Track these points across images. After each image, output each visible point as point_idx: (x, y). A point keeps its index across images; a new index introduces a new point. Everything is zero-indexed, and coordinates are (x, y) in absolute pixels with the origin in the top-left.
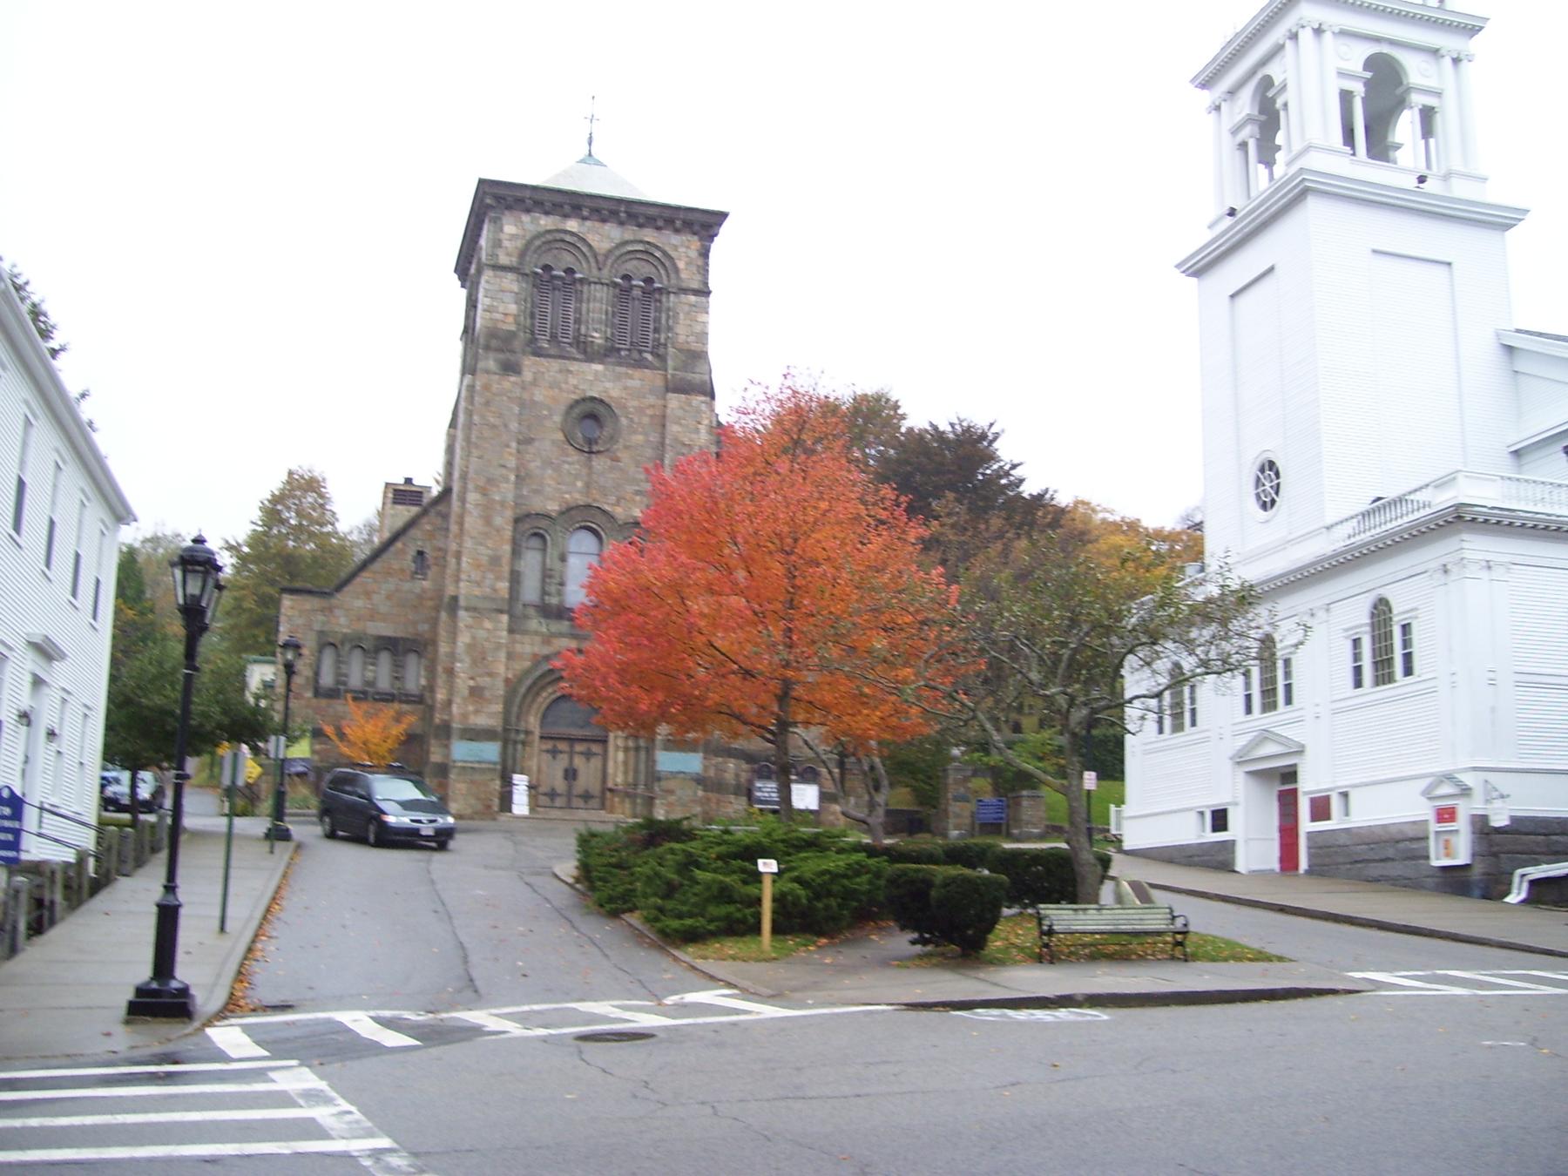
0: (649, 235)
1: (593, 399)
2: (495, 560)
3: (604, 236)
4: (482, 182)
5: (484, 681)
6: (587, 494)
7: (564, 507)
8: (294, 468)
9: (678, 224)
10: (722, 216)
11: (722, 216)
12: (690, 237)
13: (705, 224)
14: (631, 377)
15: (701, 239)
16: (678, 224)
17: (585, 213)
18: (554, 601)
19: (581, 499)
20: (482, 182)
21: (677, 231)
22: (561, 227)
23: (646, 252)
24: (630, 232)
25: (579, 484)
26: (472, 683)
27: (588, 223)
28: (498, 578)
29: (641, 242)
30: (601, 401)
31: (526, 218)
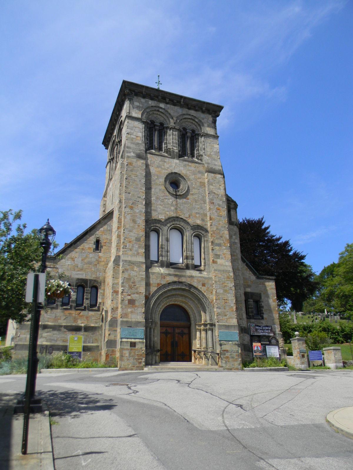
0: (192, 112)
1: (176, 173)
2: (138, 240)
3: (175, 111)
4: (124, 82)
5: (135, 296)
6: (176, 212)
7: (167, 217)
8: (291, 242)
9: (160, 97)
10: (221, 108)
11: (221, 108)
12: (208, 115)
13: (214, 110)
14: (190, 166)
15: (212, 117)
16: (167, 100)
17: (197, 108)
18: (164, 259)
19: (173, 214)
20: (124, 82)
21: (203, 112)
22: (158, 105)
23: (193, 118)
24: (185, 111)
25: (173, 208)
26: (129, 297)
27: (168, 106)
28: (139, 247)
29: (190, 115)
30: (179, 174)
31: (143, 100)
